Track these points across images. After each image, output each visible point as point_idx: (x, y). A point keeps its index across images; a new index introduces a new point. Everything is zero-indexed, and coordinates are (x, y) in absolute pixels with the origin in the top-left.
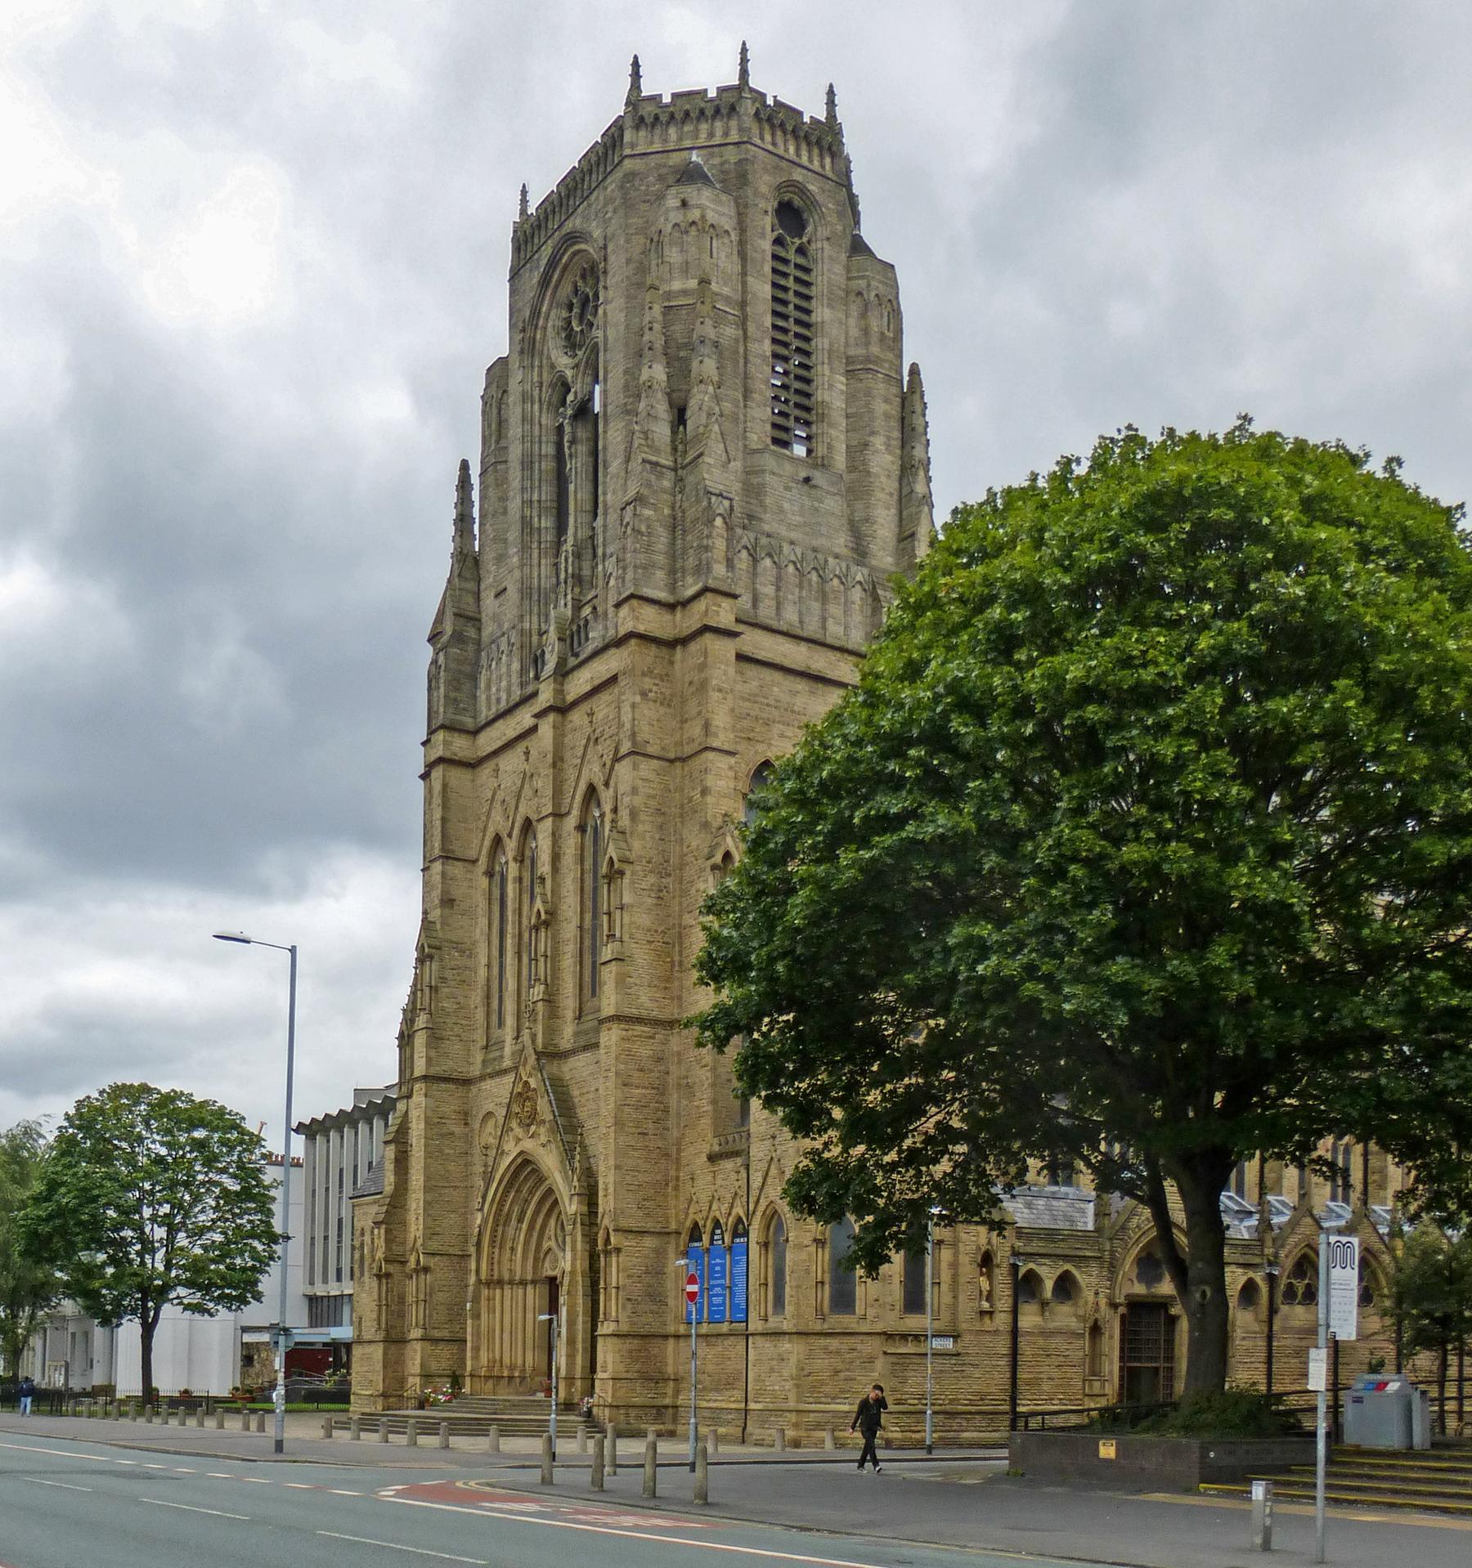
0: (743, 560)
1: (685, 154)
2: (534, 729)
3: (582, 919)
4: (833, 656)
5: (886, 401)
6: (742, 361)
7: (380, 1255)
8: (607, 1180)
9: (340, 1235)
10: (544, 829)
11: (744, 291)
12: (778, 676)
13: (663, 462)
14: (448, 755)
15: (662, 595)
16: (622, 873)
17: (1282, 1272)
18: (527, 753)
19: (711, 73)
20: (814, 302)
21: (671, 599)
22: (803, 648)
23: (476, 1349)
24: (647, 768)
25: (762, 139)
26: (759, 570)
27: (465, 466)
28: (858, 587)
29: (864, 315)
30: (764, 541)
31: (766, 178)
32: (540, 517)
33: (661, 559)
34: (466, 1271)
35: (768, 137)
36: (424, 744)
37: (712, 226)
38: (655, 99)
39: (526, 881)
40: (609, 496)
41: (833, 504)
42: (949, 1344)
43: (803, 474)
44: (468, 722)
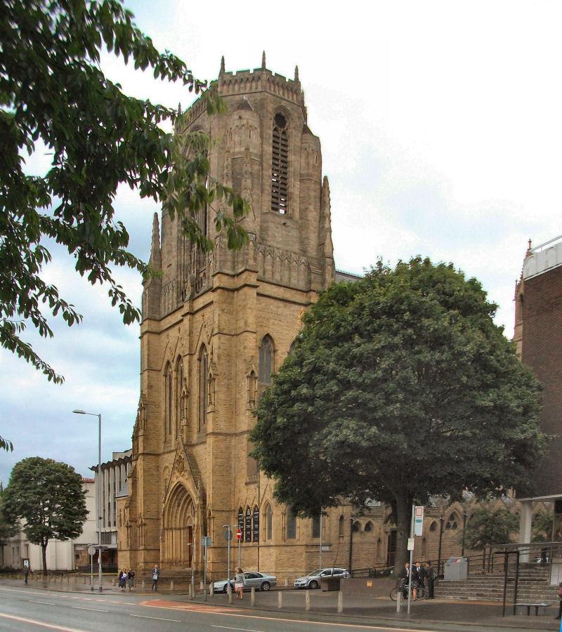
2: (182, 320)
3: (200, 394)
5: (315, 191)
7: (127, 519)
8: (209, 492)
9: (109, 509)
10: (186, 359)
11: (262, 151)
12: (272, 301)
14: (150, 330)
16: (214, 379)
17: (446, 519)
18: (179, 330)
19: (253, 64)
23: (164, 553)
24: (224, 338)
26: (266, 260)
27: (156, 215)
29: (307, 157)
30: (268, 248)
31: (272, 105)
34: (159, 525)
37: (250, 126)
38: (230, 73)
39: (179, 379)
40: (210, 231)
41: (294, 233)
42: (327, 548)
44: (157, 317)
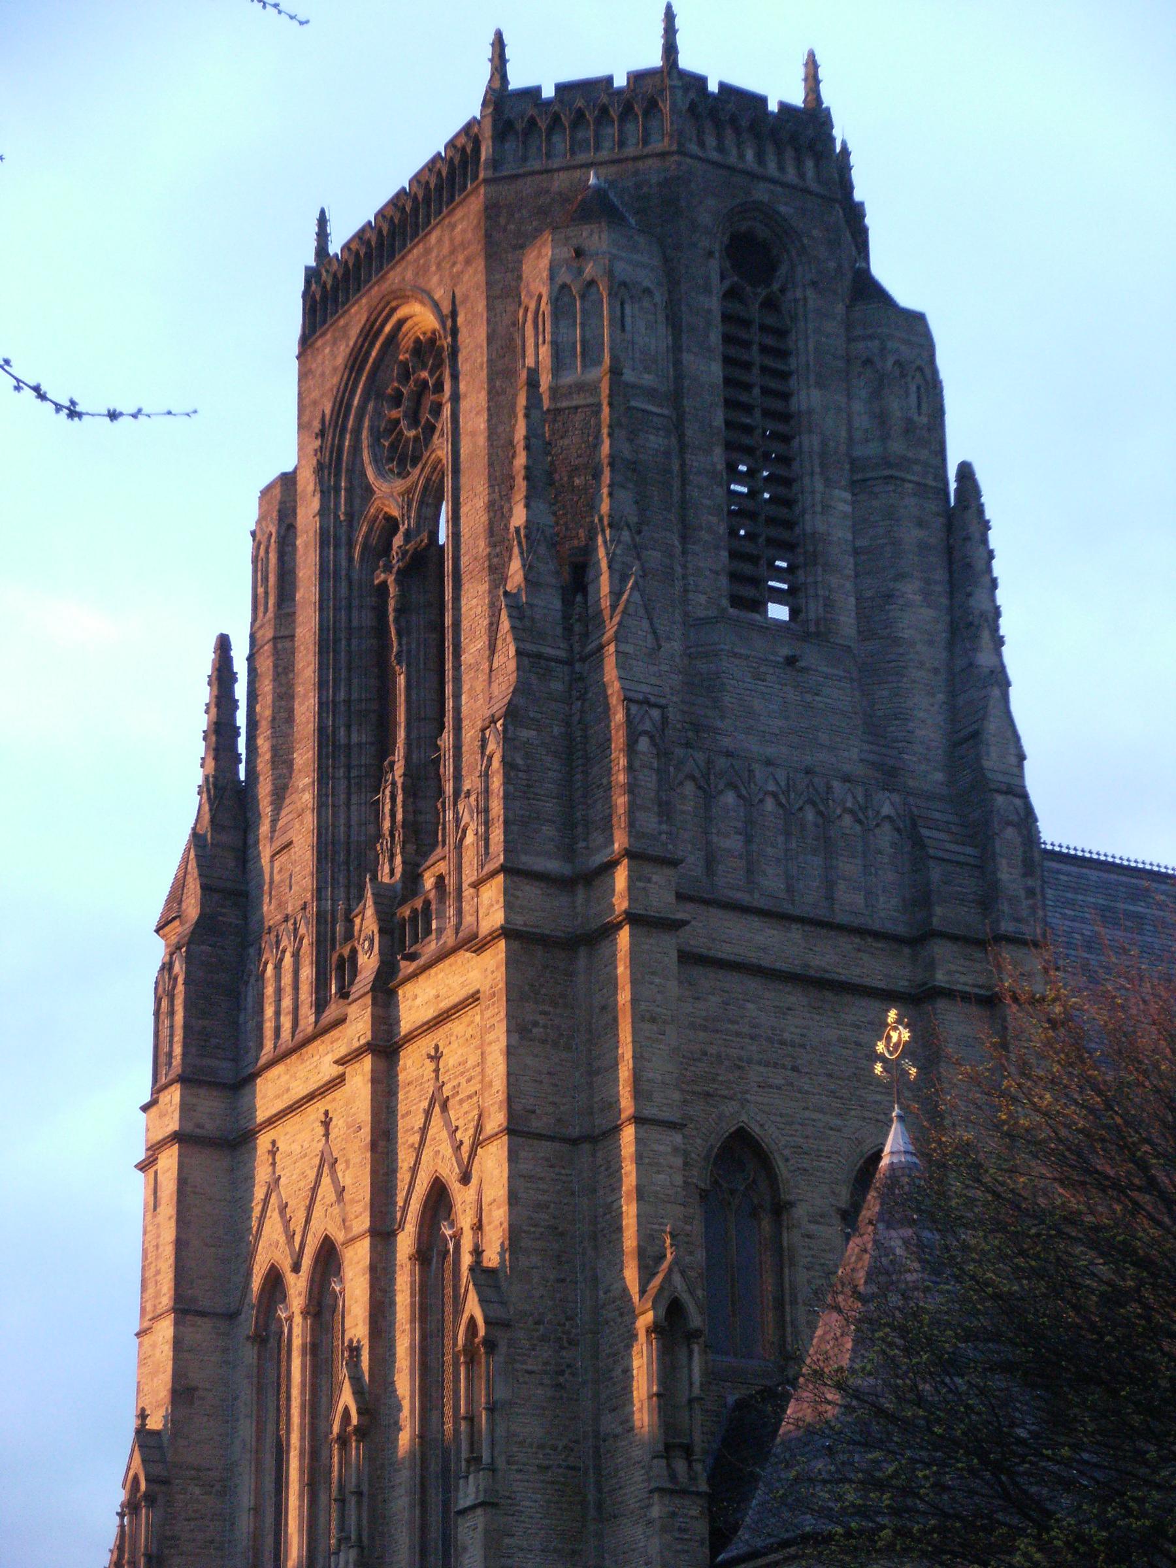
0: (688, 798)
1: (578, 174)
4: (846, 944)
5: (921, 524)
6: (676, 484)
11: (679, 377)
12: (753, 985)
13: (548, 651)
15: (552, 865)
18: (326, 1124)
20: (793, 382)
21: (566, 869)
22: (796, 933)
25: (702, 144)
27: (223, 645)
28: (887, 827)
29: (876, 394)
30: (722, 763)
31: (711, 202)
32: (349, 727)
33: (550, 807)
35: (711, 141)
36: (145, 1108)
43: (785, 651)
